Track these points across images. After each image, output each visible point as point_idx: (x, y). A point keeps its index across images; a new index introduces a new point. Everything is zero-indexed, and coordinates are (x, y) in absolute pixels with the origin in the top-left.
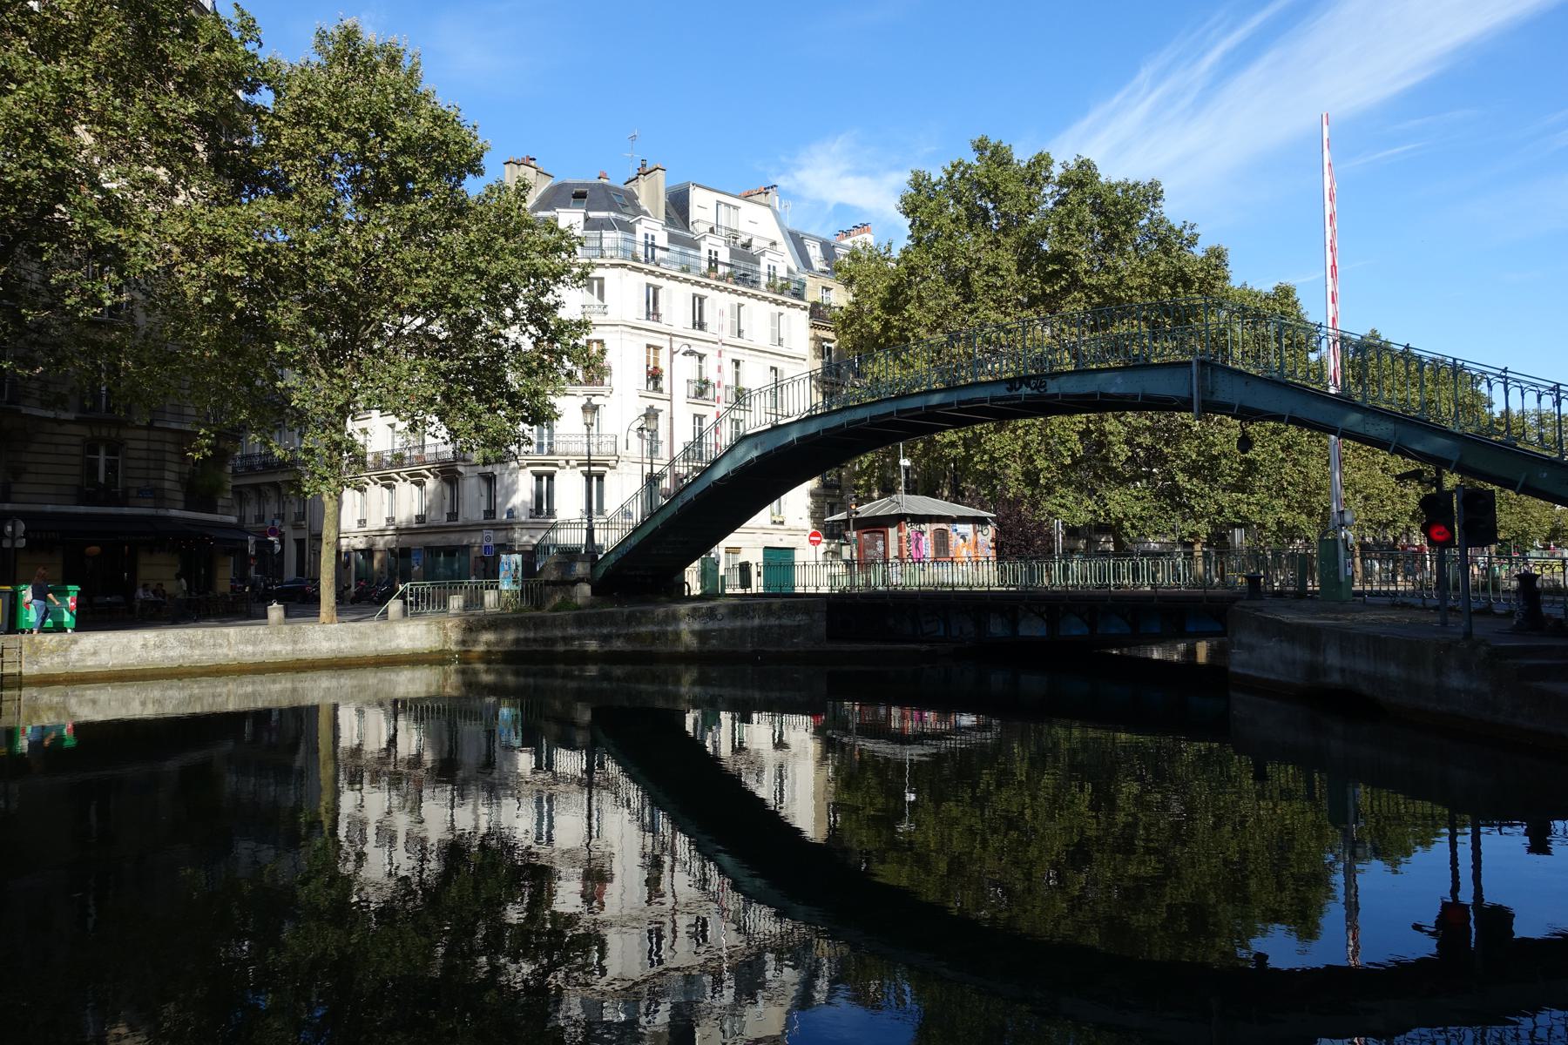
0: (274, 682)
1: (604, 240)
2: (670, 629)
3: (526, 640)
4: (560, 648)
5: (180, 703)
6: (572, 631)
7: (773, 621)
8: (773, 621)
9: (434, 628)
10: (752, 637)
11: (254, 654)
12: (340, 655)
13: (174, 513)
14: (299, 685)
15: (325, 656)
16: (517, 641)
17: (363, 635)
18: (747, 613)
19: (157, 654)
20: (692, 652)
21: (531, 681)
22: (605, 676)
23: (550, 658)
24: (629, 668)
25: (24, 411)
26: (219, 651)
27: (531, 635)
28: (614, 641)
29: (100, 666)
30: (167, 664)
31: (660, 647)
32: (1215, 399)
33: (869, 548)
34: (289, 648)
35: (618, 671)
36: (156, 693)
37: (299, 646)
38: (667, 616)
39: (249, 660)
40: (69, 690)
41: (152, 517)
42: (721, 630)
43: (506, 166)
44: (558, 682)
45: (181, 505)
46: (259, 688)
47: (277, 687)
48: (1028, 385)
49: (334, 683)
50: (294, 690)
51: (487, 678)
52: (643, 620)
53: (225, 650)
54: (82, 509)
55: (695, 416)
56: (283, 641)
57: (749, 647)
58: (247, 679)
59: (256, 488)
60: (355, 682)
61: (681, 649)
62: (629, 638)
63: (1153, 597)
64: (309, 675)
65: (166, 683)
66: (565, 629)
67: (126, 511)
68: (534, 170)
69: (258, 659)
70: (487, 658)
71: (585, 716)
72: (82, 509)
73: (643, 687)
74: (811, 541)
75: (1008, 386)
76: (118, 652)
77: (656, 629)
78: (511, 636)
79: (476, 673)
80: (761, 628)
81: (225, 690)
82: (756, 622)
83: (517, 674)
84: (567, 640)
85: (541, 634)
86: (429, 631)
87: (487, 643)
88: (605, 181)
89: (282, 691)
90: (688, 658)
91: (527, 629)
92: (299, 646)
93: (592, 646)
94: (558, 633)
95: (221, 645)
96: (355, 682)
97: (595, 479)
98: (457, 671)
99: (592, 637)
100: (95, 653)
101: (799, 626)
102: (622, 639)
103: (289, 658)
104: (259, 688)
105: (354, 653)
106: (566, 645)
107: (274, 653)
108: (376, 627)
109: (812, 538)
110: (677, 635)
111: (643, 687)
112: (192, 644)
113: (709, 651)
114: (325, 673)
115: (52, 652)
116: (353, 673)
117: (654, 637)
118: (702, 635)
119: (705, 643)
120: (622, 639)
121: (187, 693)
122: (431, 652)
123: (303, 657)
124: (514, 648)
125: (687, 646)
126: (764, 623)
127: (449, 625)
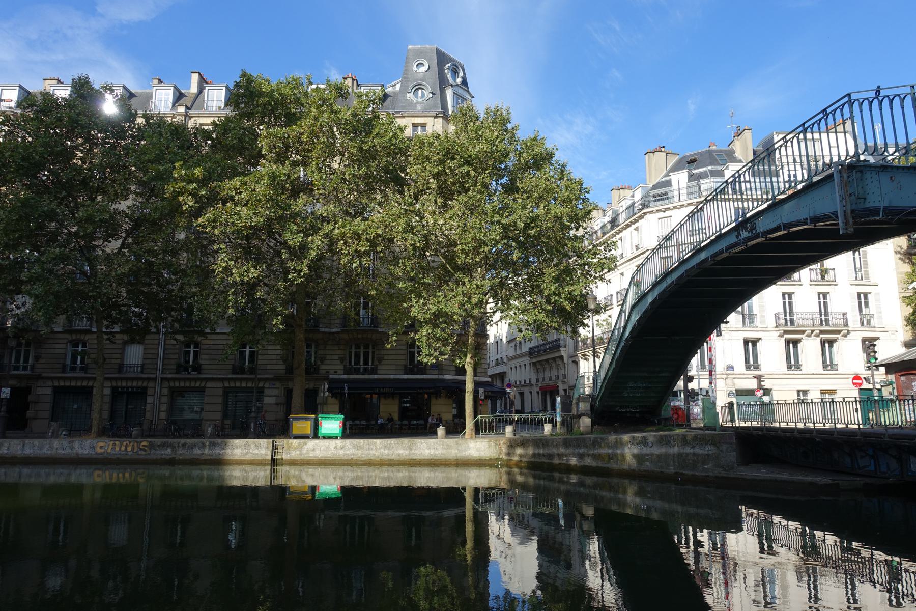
0: (399, 471)
1: (702, 186)
2: (619, 451)
3: (539, 454)
4: (556, 461)
5: (352, 480)
6: (562, 450)
7: (688, 450)
8: (688, 450)
9: (493, 444)
10: (674, 462)
11: (388, 455)
12: (435, 458)
13: (447, 377)
14: (413, 474)
15: (427, 458)
16: (534, 455)
17: (449, 447)
18: (669, 442)
19: (341, 452)
20: (634, 470)
21: (542, 482)
22: (581, 484)
23: (552, 468)
24: (595, 479)
25: (380, 330)
26: (371, 452)
27: (541, 451)
28: (586, 458)
29: (315, 457)
30: (346, 458)
31: (613, 466)
32: (868, 205)
33: (907, 388)
34: (407, 452)
35: (589, 480)
36: (340, 473)
37: (413, 451)
38: (616, 442)
39: (385, 457)
40: (302, 468)
41: (437, 379)
42: (652, 454)
43: (646, 156)
44: (556, 485)
45: (454, 372)
46: (391, 474)
47: (401, 474)
48: (746, 229)
49: (432, 474)
50: (410, 477)
51: (520, 479)
52: (602, 445)
53: (374, 452)
54: (406, 377)
55: (819, 294)
56: (404, 448)
57: (672, 470)
58: (385, 468)
59: (547, 360)
60: (444, 475)
61: (626, 467)
62: (595, 457)
63: (885, 435)
64: (418, 469)
65: (345, 468)
66: (558, 448)
67: (425, 377)
68: (664, 154)
69: (390, 457)
70: (518, 465)
71: (589, 512)
72: (406, 377)
73: (604, 494)
74: (854, 384)
75: (736, 233)
76: (324, 450)
77: (610, 451)
78: (531, 451)
79: (514, 475)
80: (680, 455)
81: (373, 474)
82: (676, 450)
83: (535, 477)
84: (560, 456)
85: (546, 451)
86: (490, 446)
87: (520, 456)
88: (714, 147)
89: (404, 477)
90: (630, 475)
91: (539, 447)
92: (413, 451)
93: (574, 461)
94: (555, 451)
95: (372, 449)
96: (444, 475)
97: (750, 344)
98: (506, 472)
99: (574, 455)
100: (314, 450)
101: (708, 455)
102: (590, 457)
103: (407, 458)
104: (391, 474)
105: (443, 457)
106: (559, 459)
107: (399, 455)
108: (457, 442)
109: (855, 381)
110: (623, 456)
111: (604, 494)
112: (358, 448)
113: (645, 471)
114: (426, 468)
115: (296, 448)
116: (443, 469)
117: (611, 457)
118: (639, 458)
119: (642, 464)
120: (590, 457)
121: (355, 474)
122: (491, 459)
123: (414, 458)
124: (532, 460)
125: (630, 466)
126: (682, 451)
127: (502, 443)
